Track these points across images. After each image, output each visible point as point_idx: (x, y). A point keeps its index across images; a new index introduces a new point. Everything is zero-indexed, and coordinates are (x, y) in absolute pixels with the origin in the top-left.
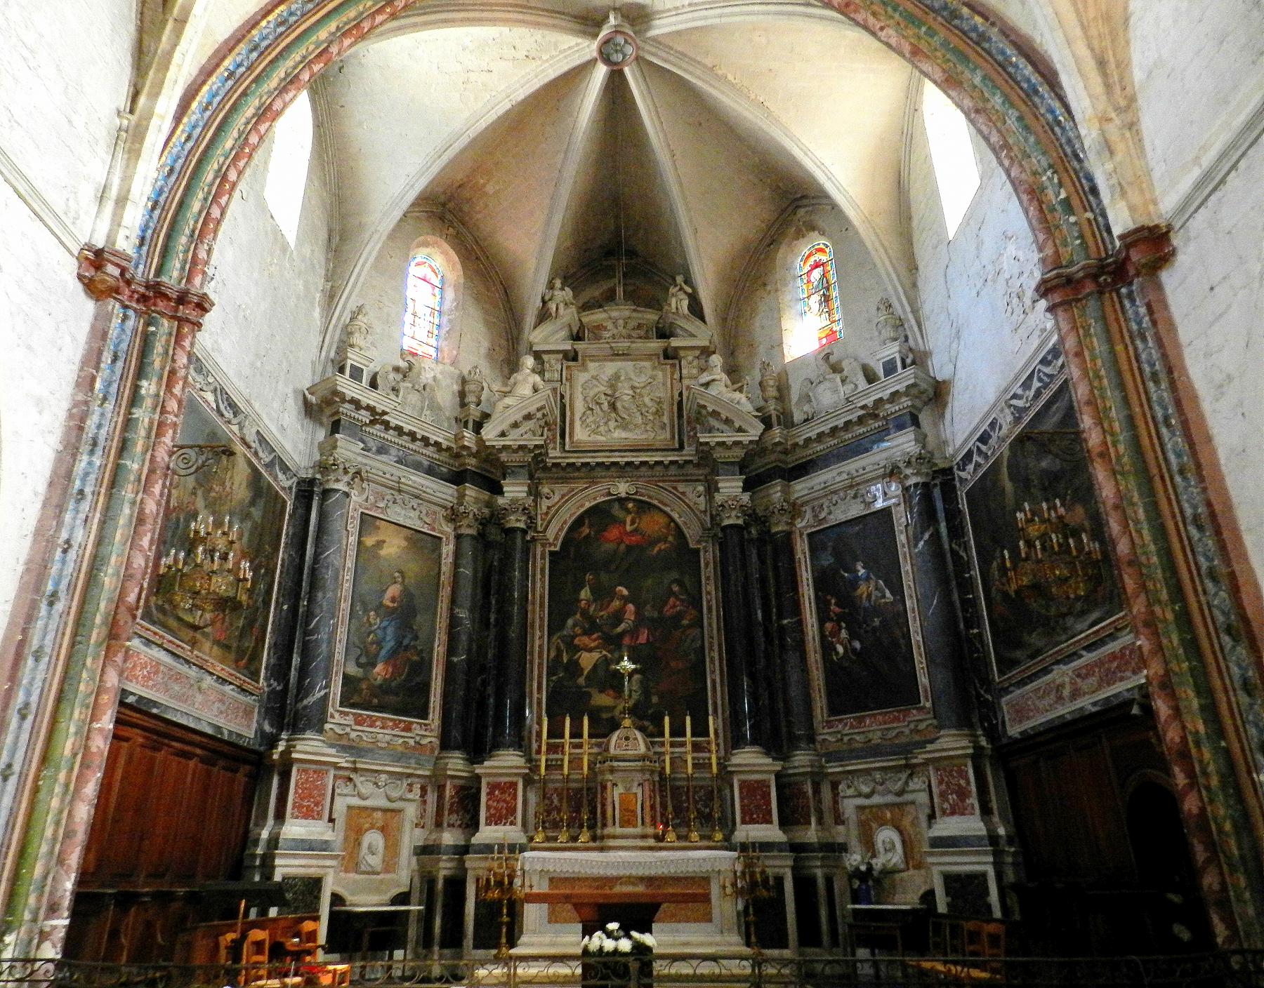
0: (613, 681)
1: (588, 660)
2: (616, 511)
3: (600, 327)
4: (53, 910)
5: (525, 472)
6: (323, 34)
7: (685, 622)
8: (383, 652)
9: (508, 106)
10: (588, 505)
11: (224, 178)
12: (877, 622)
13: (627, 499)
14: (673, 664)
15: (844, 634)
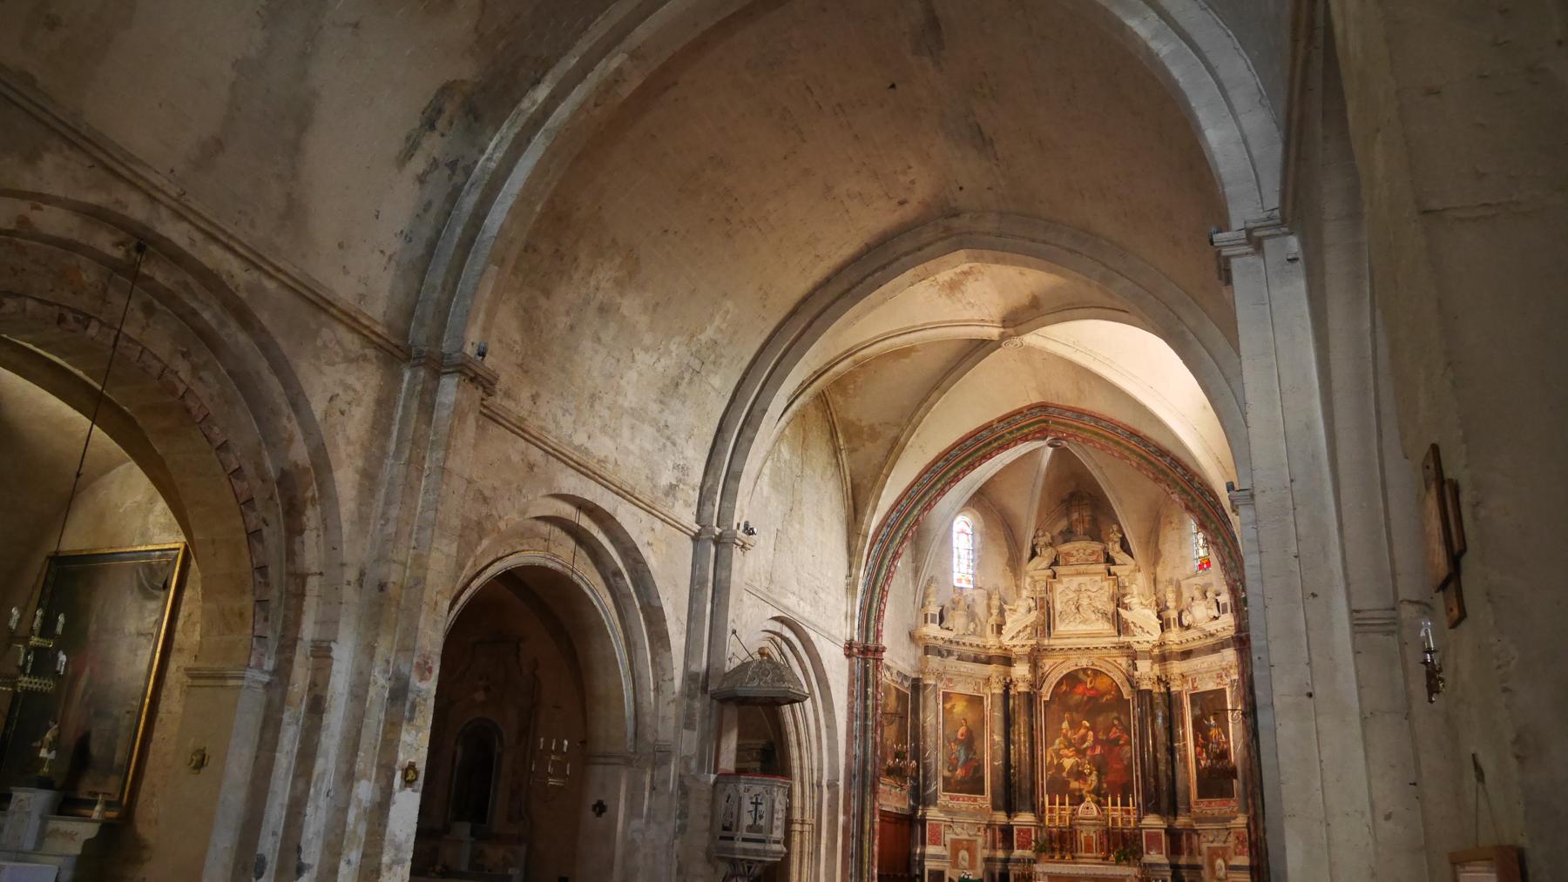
2: (1081, 675)
3: (1069, 554)
6: (915, 512)
7: (1121, 742)
9: (1002, 467)
10: (1065, 672)
13: (1086, 669)
15: (1204, 755)
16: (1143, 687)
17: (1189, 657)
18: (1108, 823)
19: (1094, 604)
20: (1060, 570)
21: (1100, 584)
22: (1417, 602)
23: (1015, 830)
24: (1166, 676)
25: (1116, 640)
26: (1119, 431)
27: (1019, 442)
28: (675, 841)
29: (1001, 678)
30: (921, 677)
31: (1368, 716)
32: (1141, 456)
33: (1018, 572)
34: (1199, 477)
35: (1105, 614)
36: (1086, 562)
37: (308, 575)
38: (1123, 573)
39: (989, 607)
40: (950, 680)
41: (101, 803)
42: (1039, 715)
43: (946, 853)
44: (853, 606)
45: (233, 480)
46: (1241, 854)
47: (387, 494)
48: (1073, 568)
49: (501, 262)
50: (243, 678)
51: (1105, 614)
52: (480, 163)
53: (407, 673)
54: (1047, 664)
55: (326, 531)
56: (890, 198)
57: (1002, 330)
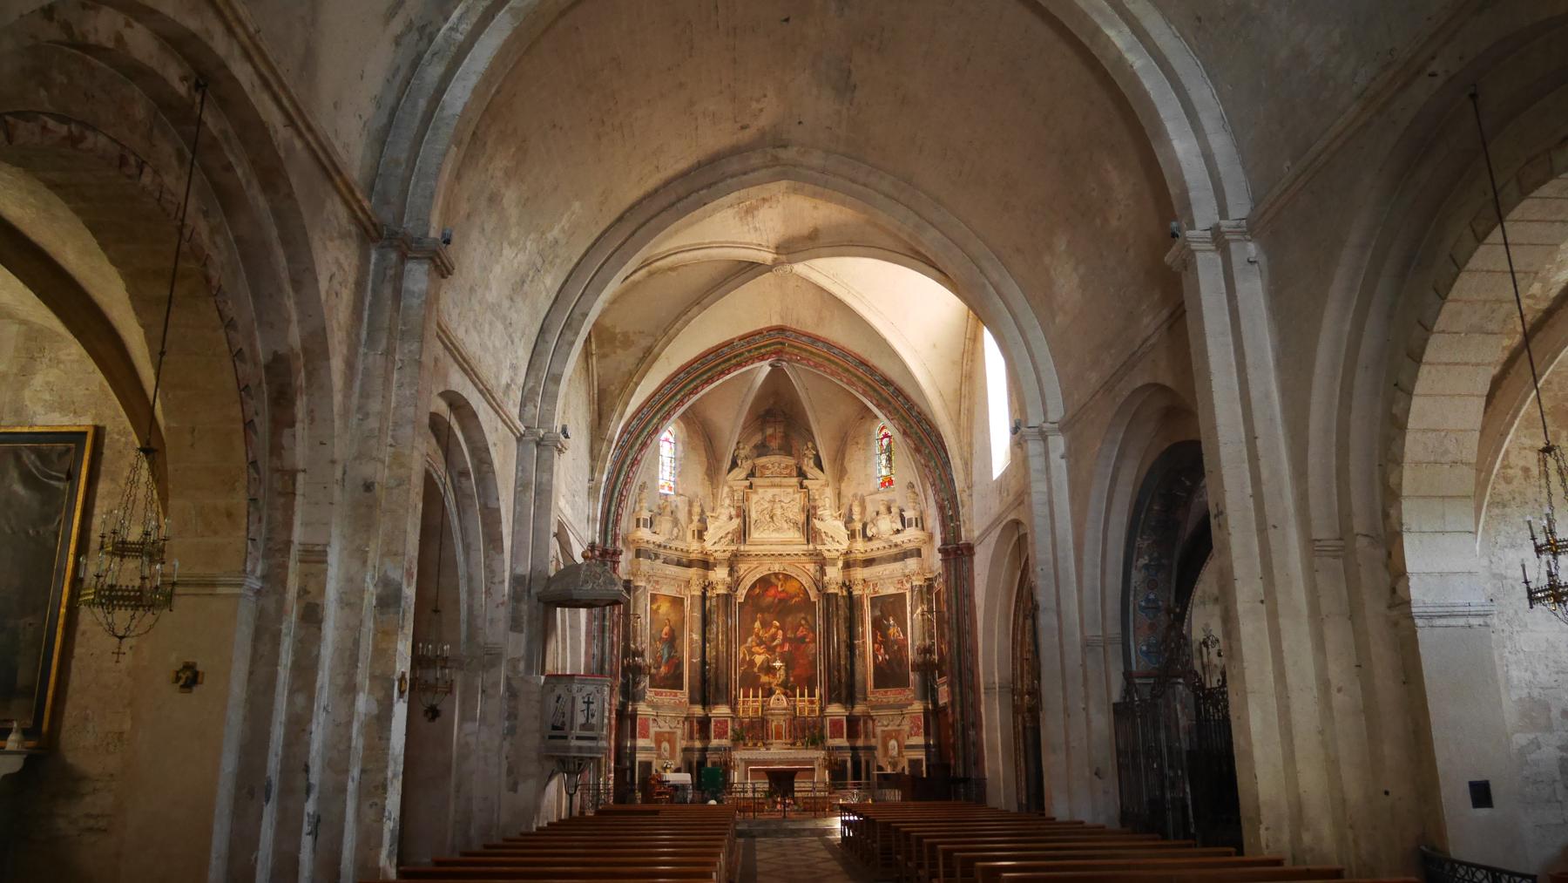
0: (769, 670)
1: (759, 659)
2: (773, 580)
3: (764, 467)
4: (610, 772)
5: (726, 563)
6: (655, 421)
7: (807, 640)
8: (664, 660)
10: (758, 576)
11: (622, 495)
12: (896, 647)
13: (779, 573)
14: (801, 661)
16: (831, 591)
17: (871, 565)
18: (796, 713)
19: (786, 514)
20: (756, 481)
21: (791, 496)
22: (1366, 536)
23: (712, 721)
24: (850, 581)
25: (805, 547)
26: (849, 359)
27: (756, 360)
28: (504, 743)
29: (701, 581)
30: (632, 578)
31: (1324, 617)
32: (867, 383)
33: (715, 481)
34: (918, 407)
35: (796, 524)
36: (780, 475)
37: (298, 471)
38: (814, 487)
39: (690, 513)
40: (657, 582)
41: (17, 732)
42: (733, 616)
43: (653, 745)
44: (595, 510)
45: (237, 364)
46: (917, 734)
47: (362, 386)
48: (768, 480)
49: (459, 144)
50: (240, 585)
51: (796, 524)
52: (442, 31)
53: (400, 580)
54: (743, 568)
55: (311, 424)
56: (736, 122)
57: (776, 256)
